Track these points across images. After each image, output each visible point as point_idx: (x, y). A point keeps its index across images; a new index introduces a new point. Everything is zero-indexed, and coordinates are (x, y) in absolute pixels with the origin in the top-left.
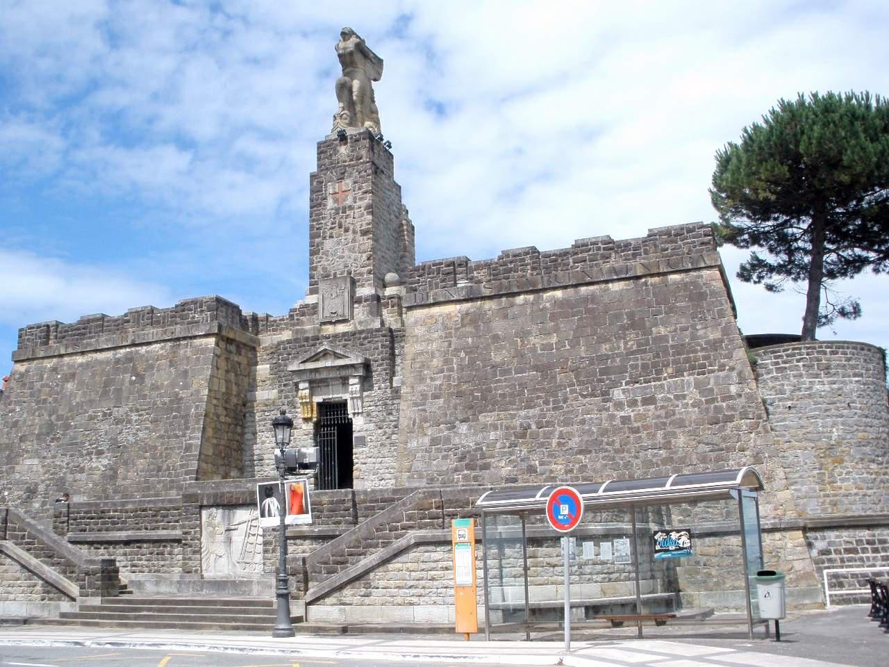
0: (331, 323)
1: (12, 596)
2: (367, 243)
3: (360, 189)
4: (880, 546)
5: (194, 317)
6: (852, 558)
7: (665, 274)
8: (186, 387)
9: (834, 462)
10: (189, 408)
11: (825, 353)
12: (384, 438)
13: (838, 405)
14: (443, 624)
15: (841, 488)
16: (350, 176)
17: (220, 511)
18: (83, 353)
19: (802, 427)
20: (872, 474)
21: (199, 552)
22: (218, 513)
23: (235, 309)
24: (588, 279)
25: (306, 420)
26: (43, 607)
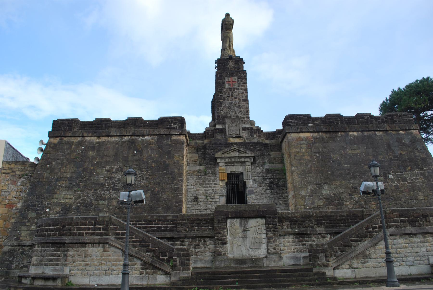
0: (232, 137)
1: (115, 272)
12: (263, 191)
14: (371, 277)
17: (238, 220)
22: (237, 222)
26: (142, 279)
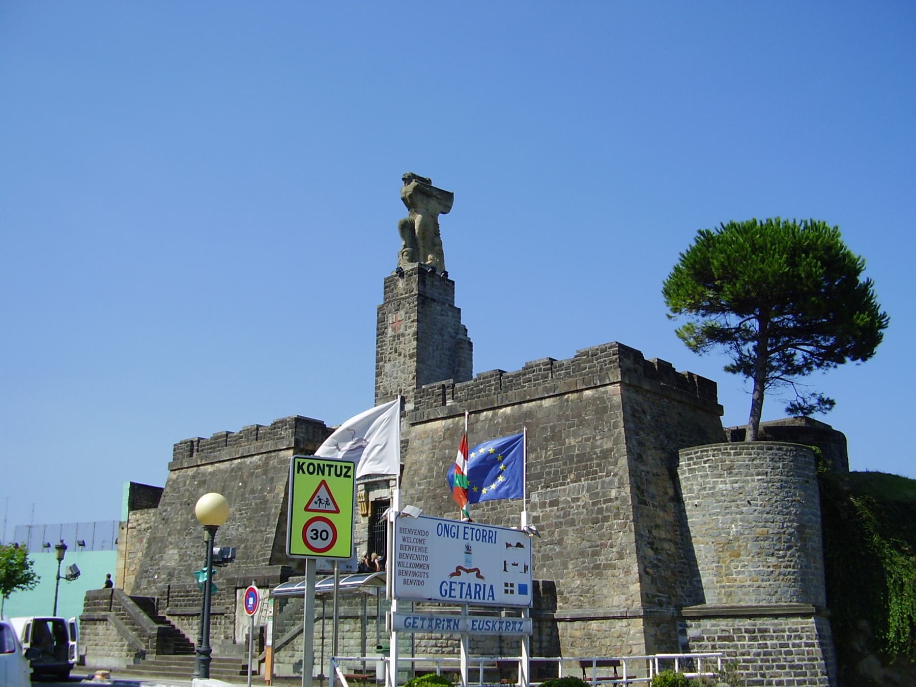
2: (412, 364)
4: (759, 635)
6: (725, 645)
7: (582, 390)
8: (271, 491)
9: (731, 556)
10: (271, 508)
11: (729, 454)
13: (738, 502)
15: (736, 580)
18: (212, 463)
19: (705, 523)
20: (769, 567)
21: (234, 623)
23: (638, 355)
24: (528, 398)
25: (364, 515)
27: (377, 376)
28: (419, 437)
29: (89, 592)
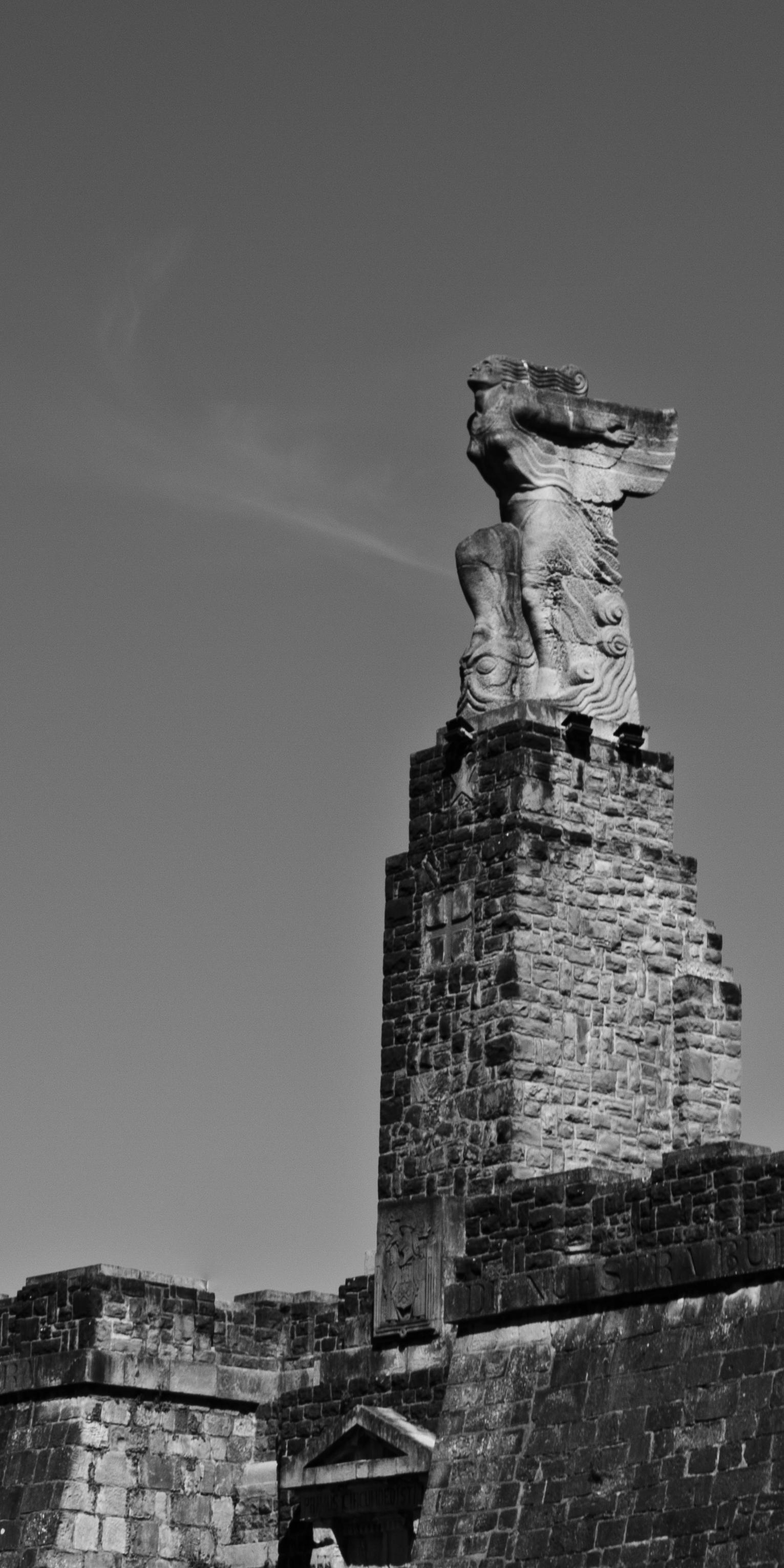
3: (488, 915)
5: (46, 1334)
16: (469, 874)
27: (384, 1120)
28: (478, 1373)
29: (388, 859)
